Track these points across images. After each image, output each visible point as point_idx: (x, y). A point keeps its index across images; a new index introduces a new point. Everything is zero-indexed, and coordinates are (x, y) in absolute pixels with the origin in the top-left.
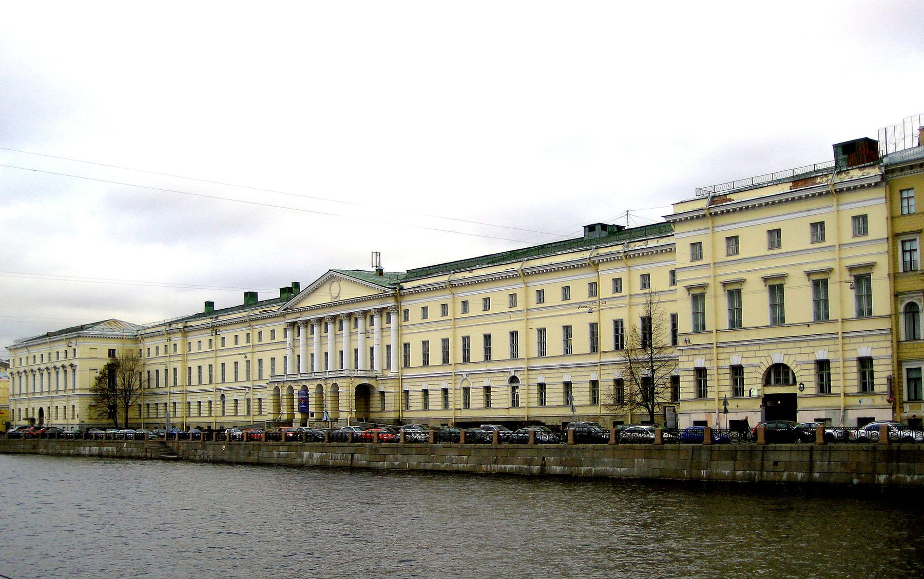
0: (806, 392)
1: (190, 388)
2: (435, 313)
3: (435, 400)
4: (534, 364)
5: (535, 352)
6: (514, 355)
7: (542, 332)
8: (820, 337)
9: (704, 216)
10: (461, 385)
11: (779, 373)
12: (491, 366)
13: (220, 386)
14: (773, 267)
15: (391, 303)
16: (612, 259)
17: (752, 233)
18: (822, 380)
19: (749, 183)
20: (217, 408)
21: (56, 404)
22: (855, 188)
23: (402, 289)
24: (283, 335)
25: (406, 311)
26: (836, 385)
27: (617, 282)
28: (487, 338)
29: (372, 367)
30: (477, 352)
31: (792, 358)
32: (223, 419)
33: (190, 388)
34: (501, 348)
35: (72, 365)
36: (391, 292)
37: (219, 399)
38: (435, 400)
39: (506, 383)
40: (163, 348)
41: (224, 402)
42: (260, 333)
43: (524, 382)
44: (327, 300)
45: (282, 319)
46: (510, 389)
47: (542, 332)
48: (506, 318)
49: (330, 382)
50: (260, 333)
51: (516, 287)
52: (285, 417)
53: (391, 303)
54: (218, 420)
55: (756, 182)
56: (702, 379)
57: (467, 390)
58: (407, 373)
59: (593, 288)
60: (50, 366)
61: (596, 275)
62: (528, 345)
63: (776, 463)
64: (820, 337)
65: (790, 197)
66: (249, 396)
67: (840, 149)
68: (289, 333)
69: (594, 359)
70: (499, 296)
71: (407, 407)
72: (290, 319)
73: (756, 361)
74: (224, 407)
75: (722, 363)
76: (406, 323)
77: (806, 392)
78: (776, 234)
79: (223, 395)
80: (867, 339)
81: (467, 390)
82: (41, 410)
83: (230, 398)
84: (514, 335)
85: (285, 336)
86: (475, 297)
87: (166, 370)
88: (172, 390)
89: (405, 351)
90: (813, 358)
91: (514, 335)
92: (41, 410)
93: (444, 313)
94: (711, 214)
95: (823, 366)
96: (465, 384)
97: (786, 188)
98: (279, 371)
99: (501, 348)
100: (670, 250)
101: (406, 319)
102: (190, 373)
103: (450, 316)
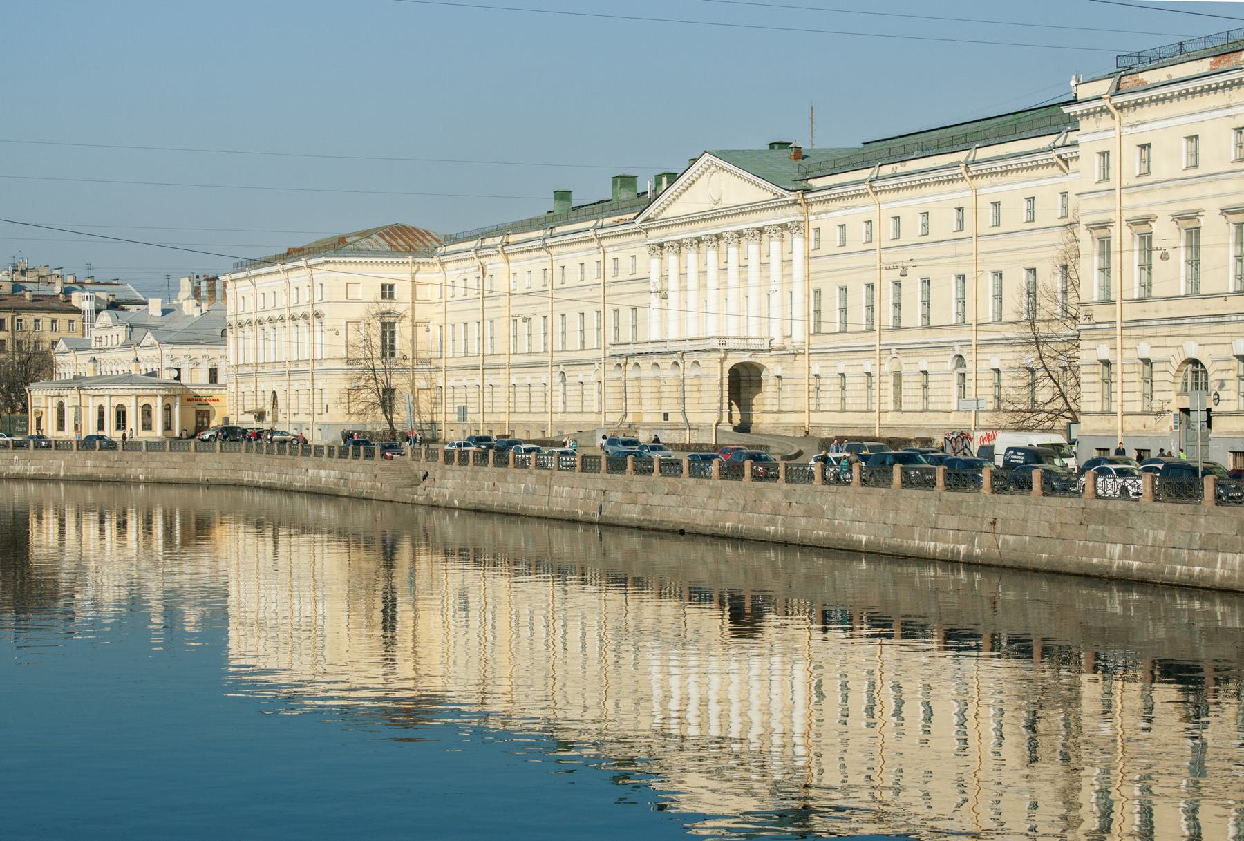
9: (1103, 111)
31: (1209, 349)
53: (790, 215)
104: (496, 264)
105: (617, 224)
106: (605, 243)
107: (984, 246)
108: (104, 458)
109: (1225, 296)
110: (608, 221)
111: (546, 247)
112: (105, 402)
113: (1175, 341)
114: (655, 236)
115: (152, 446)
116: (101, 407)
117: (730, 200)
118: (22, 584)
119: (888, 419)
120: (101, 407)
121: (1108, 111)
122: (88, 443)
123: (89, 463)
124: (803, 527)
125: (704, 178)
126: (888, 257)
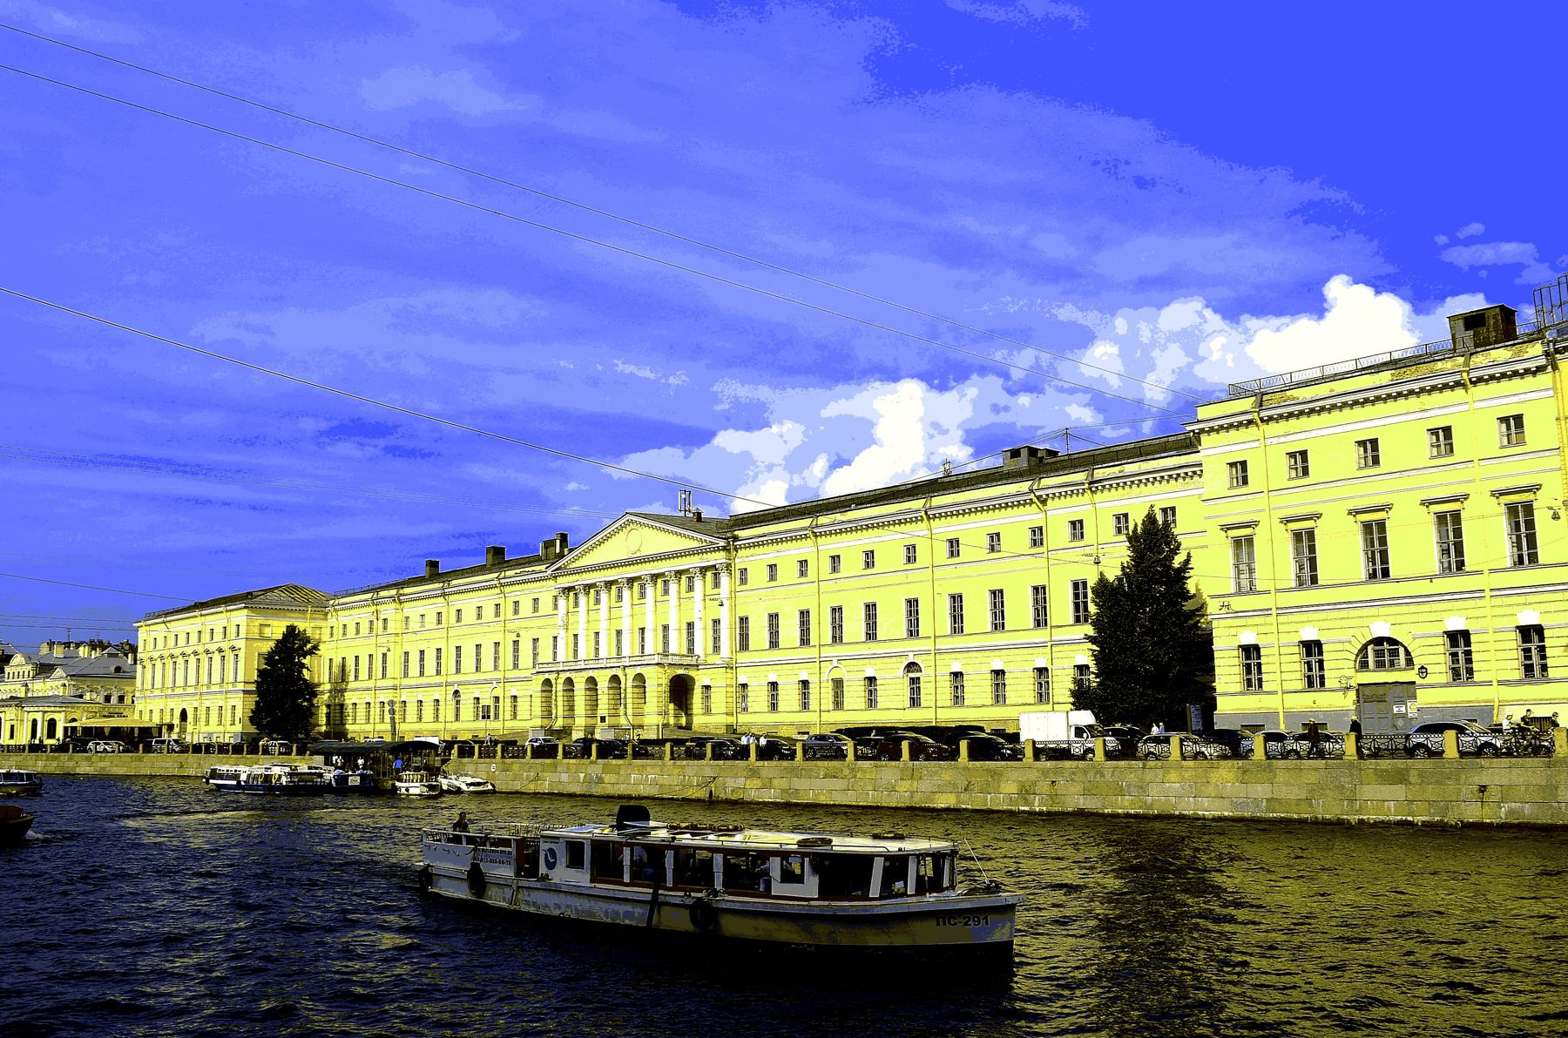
0: (1430, 680)
1: (405, 682)
2: (788, 571)
3: (789, 696)
4: (943, 644)
5: (510, 665)
6: (913, 632)
7: (956, 600)
8: (1454, 596)
9: (1250, 422)
10: (829, 673)
11: (1385, 650)
12: (874, 648)
13: (452, 679)
14: (1443, 483)
15: (719, 558)
16: (1072, 490)
17: (1331, 441)
18: (1249, 672)
19: (1317, 374)
20: (447, 711)
21: (207, 704)
22: (1504, 375)
23: (736, 538)
24: (551, 605)
25: (744, 571)
26: (1011, 694)
27: (1077, 526)
28: (871, 609)
29: (691, 650)
30: (854, 626)
31: (1405, 628)
32: (456, 725)
33: (405, 682)
34: (892, 622)
35: (233, 648)
36: (722, 543)
37: (450, 696)
38: (789, 696)
39: (901, 671)
40: (367, 625)
41: (458, 702)
42: (516, 603)
43: (931, 671)
44: (623, 555)
45: (552, 582)
46: (907, 681)
47: (956, 600)
48: (900, 577)
49: (563, 676)
50: (516, 603)
51: (804, 549)
52: (559, 724)
53: (719, 558)
54: (826, 717)
55: (1329, 371)
56: (1313, 660)
57: (838, 684)
58: (743, 657)
59: (1037, 536)
60: (166, 653)
61: (1042, 515)
62: (935, 617)
63: (1483, 789)
64: (1454, 596)
65: (1393, 390)
66: (498, 692)
67: (1461, 323)
68: (562, 602)
69: (1042, 635)
70: (889, 545)
71: (745, 709)
72: (565, 581)
73: (1345, 635)
74: (458, 709)
75: (1285, 638)
76: (743, 587)
77: (1430, 680)
78: (1299, 458)
79: (456, 692)
80: (1531, 598)
81: (838, 684)
82: (184, 714)
83: (467, 697)
84: (912, 604)
85: (556, 607)
86: (851, 547)
87: (516, 643)
88: (509, 675)
89: (715, 631)
90: (1297, 638)
91: (912, 604)
92: (184, 714)
93: (497, 614)
94: (1262, 420)
95: (1459, 639)
96: (836, 674)
97: (1385, 377)
98: (545, 655)
99: (892, 622)
100: (1196, 471)
101: (743, 581)
102: (407, 661)
103: (502, 617)
104: (388, 610)
105: (517, 575)
106: (507, 589)
107: (938, 573)
108: (55, 759)
109: (1431, 578)
110: (509, 573)
111: (444, 595)
112: (38, 716)
113: (1233, 631)
114: (565, 581)
115: (20, 749)
116: (35, 721)
117: (646, 551)
118: (291, 883)
119: (509, 724)
120: (35, 721)
121: (1464, 385)
122: (36, 748)
123: (40, 763)
124: (1327, 808)
125: (622, 535)
126: (510, 626)
